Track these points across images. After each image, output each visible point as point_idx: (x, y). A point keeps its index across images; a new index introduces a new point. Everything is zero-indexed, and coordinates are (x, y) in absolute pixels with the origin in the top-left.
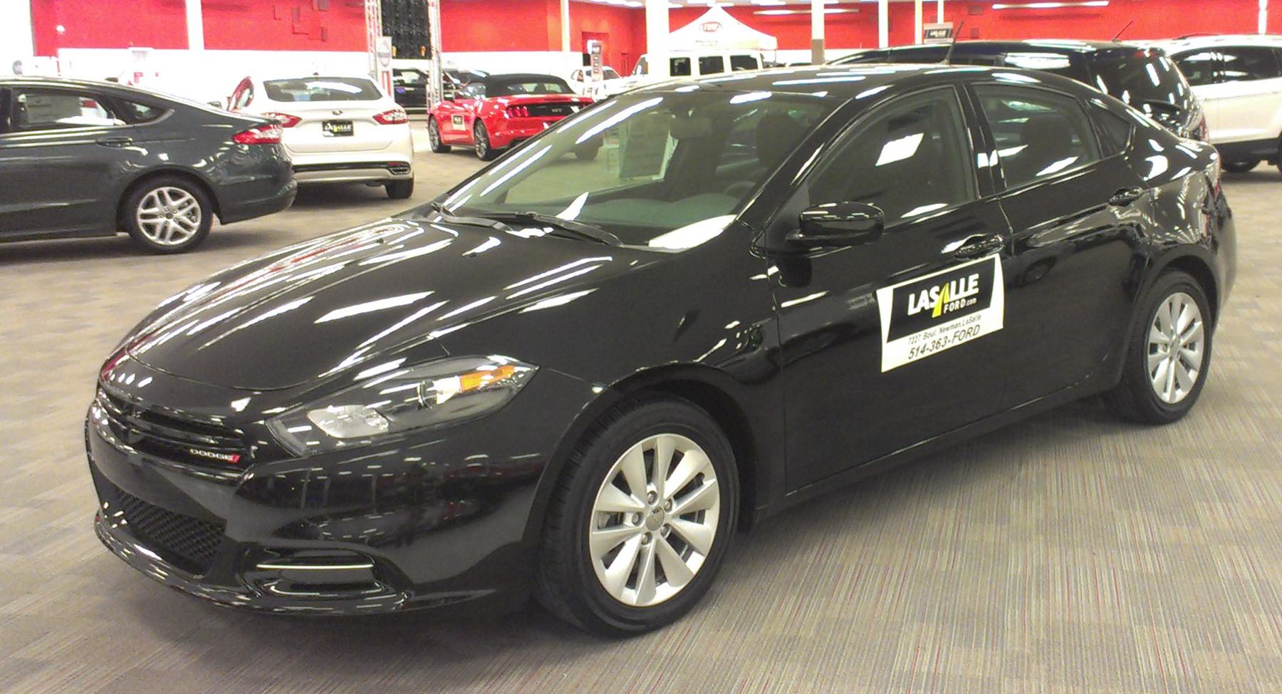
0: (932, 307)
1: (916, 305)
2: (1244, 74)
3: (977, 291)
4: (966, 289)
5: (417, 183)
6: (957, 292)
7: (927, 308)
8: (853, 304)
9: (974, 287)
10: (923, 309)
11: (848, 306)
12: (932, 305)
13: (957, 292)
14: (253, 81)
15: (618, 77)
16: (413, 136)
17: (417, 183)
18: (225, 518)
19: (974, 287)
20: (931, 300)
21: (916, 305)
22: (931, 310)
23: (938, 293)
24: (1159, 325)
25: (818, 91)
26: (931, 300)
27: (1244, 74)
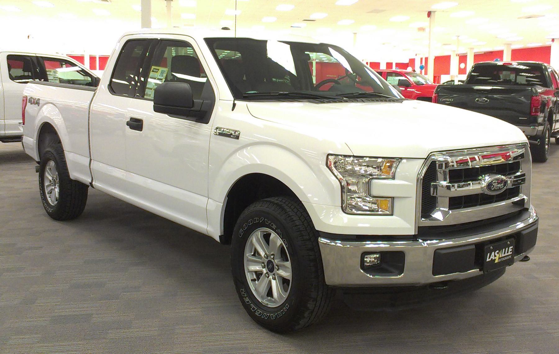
0: (495, 258)
1: (489, 258)
2: (365, 68)
3: (511, 253)
4: (508, 252)
5: (146, 22)
6: (504, 253)
7: (493, 259)
8: (173, 54)
9: (510, 252)
10: (492, 259)
11: (175, 54)
12: (495, 258)
13: (504, 253)
14: (454, 161)
15: (474, 63)
16: (408, 200)
17: (146, 22)
18: (239, 139)
19: (510, 252)
20: (495, 256)
21: (489, 258)
22: (495, 260)
23: (498, 253)
24: (369, 166)
25: (175, 73)
26: (495, 256)
27: (365, 68)
